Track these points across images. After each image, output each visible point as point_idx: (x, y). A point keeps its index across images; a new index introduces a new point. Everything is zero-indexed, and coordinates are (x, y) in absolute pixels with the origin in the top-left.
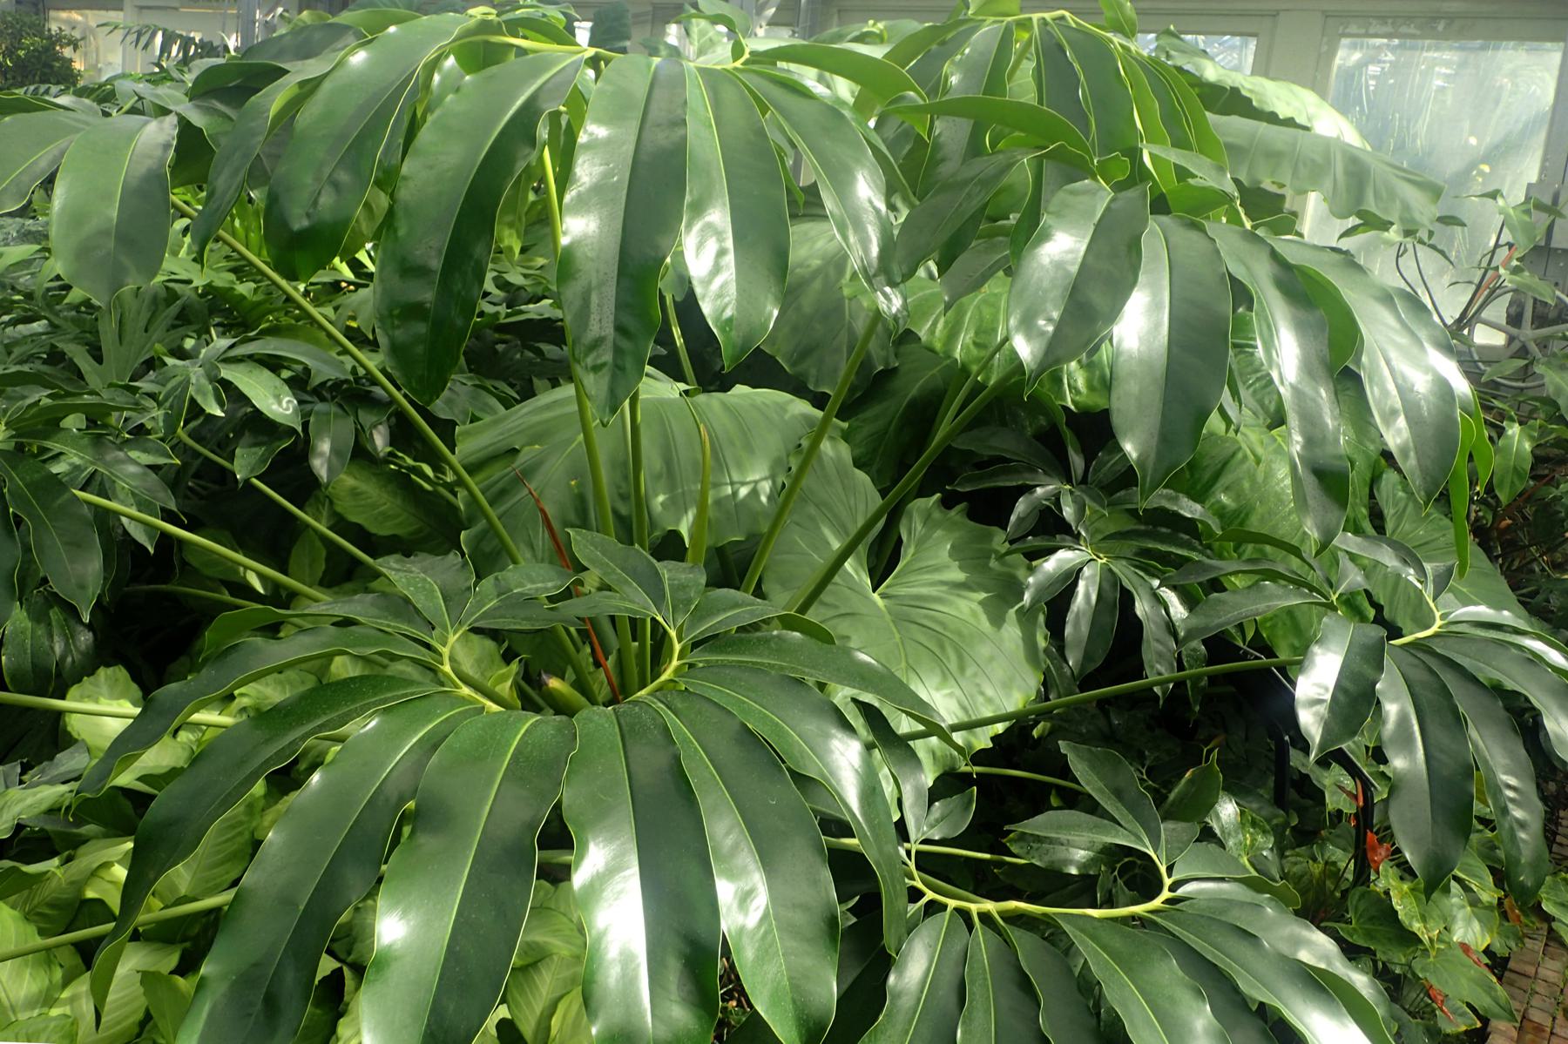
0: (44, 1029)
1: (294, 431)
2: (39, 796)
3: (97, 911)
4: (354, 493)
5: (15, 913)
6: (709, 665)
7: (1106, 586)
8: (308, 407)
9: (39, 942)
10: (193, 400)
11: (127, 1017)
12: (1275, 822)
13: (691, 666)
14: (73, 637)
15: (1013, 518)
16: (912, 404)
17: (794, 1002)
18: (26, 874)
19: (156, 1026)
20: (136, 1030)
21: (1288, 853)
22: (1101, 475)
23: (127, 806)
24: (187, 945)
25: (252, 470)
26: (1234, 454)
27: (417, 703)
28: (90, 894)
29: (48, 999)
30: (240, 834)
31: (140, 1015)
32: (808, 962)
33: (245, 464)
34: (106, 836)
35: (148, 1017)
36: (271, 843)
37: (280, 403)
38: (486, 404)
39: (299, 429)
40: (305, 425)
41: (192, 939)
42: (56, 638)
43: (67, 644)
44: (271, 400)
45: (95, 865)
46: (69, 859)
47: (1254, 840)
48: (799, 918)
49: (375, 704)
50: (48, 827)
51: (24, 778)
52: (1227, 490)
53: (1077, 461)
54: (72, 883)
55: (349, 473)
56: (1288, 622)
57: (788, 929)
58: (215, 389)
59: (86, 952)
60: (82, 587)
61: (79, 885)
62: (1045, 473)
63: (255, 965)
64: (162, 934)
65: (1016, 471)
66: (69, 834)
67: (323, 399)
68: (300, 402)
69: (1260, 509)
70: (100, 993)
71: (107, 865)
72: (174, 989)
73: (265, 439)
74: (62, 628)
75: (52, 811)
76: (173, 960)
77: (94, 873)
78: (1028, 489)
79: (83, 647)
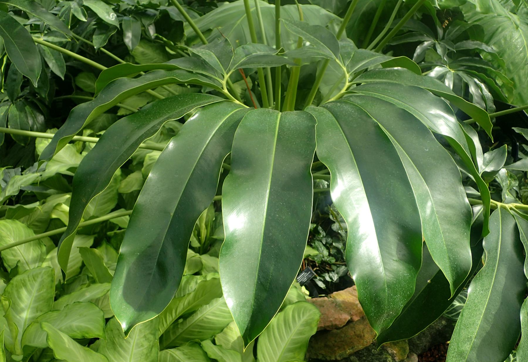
0: (40, 273)
1: (117, 27)
2: (28, 178)
3: (58, 223)
4: (143, 54)
5: (23, 225)
6: (368, 84)
7: (457, 81)
8: (121, 18)
9: (35, 236)
10: (74, 16)
11: (74, 265)
12: (518, 176)
13: (358, 85)
14: (36, 118)
15: (415, 55)
16: (364, 14)
17: (449, 258)
18: (26, 209)
19: (87, 269)
20: (79, 270)
21: (522, 188)
22: (450, 36)
23: (65, 181)
24: (96, 235)
25: (101, 44)
26: (497, 29)
27: (217, 104)
28: (54, 216)
29: (41, 259)
30: (113, 191)
31: (80, 264)
32: (455, 236)
33: (97, 42)
34: (58, 193)
35: (83, 265)
36: (151, 179)
37: (109, 15)
38: (194, 16)
39: (118, 26)
40: (121, 25)
41: (104, 235)
42: (29, 118)
43: (34, 120)
44: (106, 14)
45: (54, 205)
46: (44, 203)
47: (510, 183)
48: (449, 212)
49: (195, 106)
50: (34, 191)
51: (23, 173)
52: (495, 44)
53: (440, 32)
54: (46, 212)
55: (140, 46)
56: (519, 98)
57: (446, 219)
58: (82, 10)
59: (56, 240)
60: (32, 70)
61: (49, 213)
62: (427, 36)
63: (150, 246)
64: (86, 232)
65: (415, 35)
66: (42, 193)
67: (125, 15)
68: (118, 16)
69: (508, 52)
70: (63, 259)
71: (59, 204)
72: (94, 254)
73: (104, 31)
74: (31, 114)
75: (34, 184)
76: (91, 242)
77: (55, 208)
78: (421, 43)
79: (40, 122)
